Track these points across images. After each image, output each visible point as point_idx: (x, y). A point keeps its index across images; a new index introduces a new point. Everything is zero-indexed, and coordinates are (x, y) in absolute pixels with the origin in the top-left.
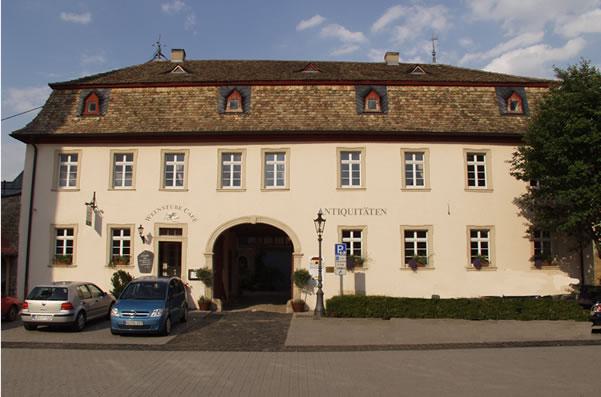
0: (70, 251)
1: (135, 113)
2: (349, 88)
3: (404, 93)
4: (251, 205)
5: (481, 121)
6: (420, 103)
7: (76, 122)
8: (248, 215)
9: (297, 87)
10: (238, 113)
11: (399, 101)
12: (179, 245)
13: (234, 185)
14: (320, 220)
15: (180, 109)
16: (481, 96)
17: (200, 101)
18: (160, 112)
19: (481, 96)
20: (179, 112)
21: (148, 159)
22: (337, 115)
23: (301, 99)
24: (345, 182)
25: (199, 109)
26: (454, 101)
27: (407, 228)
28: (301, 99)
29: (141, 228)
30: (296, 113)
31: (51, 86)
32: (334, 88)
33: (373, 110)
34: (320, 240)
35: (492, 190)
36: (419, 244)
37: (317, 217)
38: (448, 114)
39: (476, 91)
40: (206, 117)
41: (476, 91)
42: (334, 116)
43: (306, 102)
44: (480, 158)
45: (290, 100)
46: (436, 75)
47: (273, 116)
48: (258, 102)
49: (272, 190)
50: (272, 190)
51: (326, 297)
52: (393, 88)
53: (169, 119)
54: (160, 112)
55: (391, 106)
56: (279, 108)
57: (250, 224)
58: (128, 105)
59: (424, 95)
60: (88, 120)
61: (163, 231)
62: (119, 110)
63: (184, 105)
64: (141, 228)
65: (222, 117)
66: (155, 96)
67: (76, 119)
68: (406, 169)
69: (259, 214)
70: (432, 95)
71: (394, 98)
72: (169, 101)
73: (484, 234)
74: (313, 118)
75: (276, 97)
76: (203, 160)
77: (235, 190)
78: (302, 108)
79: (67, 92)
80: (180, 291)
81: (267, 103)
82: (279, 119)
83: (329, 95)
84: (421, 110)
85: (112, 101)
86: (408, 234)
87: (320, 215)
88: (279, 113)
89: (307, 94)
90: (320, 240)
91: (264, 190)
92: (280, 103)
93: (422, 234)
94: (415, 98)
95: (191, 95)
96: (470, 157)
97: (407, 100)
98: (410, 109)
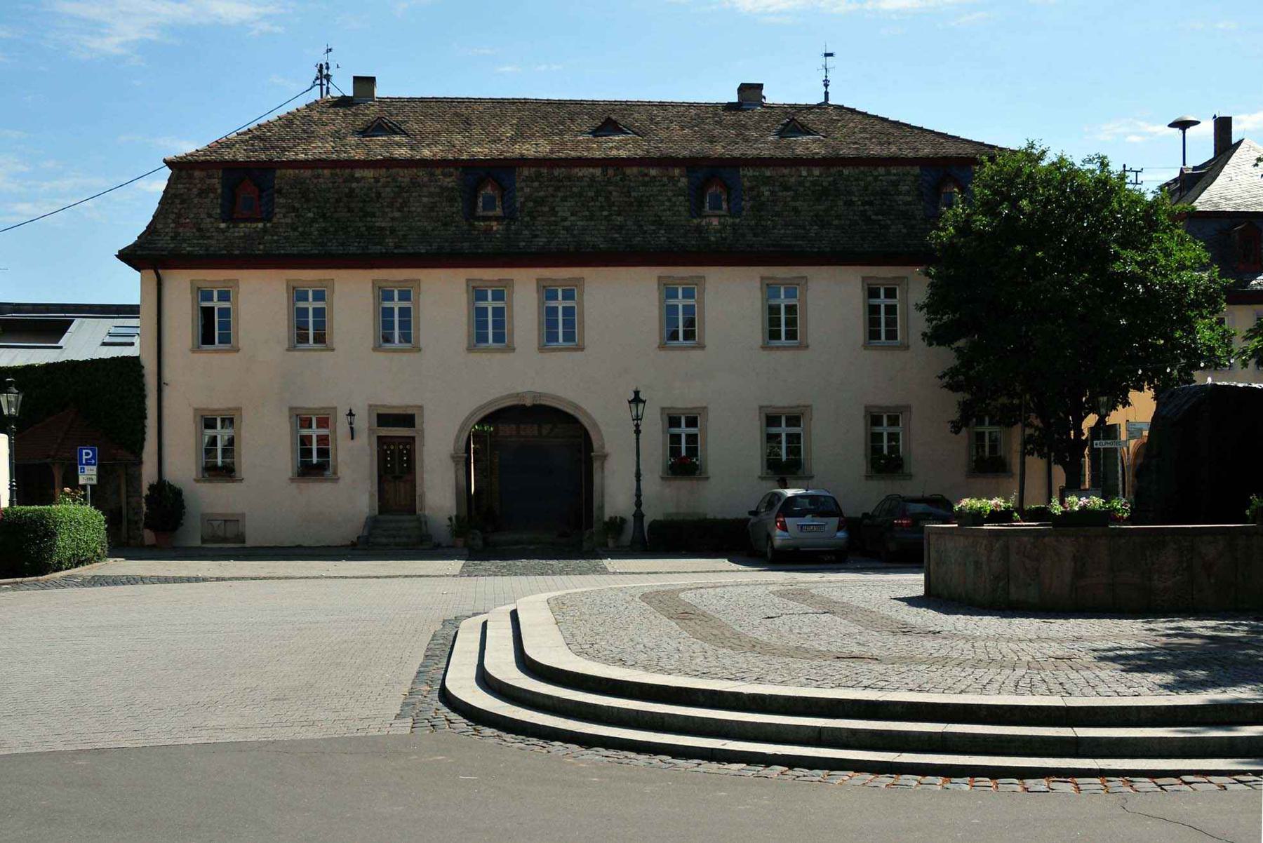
0: (323, 453)
1: (324, 216)
2: (677, 172)
3: (768, 181)
4: (527, 372)
5: (893, 229)
6: (794, 199)
7: (223, 231)
8: (520, 390)
9: (591, 170)
10: (497, 219)
11: (760, 195)
12: (413, 438)
13: (685, 338)
14: (637, 399)
15: (399, 210)
16: (895, 184)
17: (431, 195)
18: (366, 214)
19: (895, 184)
20: (397, 214)
21: (352, 295)
22: (659, 222)
23: (598, 194)
24: (303, 338)
25: (432, 209)
26: (850, 193)
27: (770, 411)
28: (598, 194)
29: (351, 414)
30: (591, 218)
31: (169, 163)
32: (653, 172)
33: (490, 214)
34: (638, 432)
35: (807, 347)
36: (688, 436)
37: (633, 396)
38: (838, 217)
39: (888, 173)
40: (445, 225)
41: (888, 173)
42: (653, 223)
43: (607, 199)
44: (890, 293)
45: (580, 195)
46: (416, 140)
47: (556, 223)
48: (528, 198)
49: (778, 348)
50: (778, 348)
51: (647, 520)
52: (751, 173)
53: (382, 229)
54: (366, 214)
55: (747, 204)
56: (563, 210)
57: (524, 406)
58: (308, 201)
59: (801, 184)
60: (243, 228)
61: (385, 419)
62: (294, 209)
63: (405, 203)
64: (351, 414)
65: (471, 225)
66: (354, 185)
67: (223, 225)
68: (668, 314)
69: (538, 387)
70: (814, 183)
71: (751, 189)
72: (379, 195)
73: (894, 421)
74: (621, 227)
75: (557, 189)
76: (442, 295)
77: (403, 351)
78: (602, 208)
79: (197, 173)
80: (779, 499)
81: (541, 202)
82: (566, 229)
83: (645, 184)
84: (795, 210)
85: (279, 191)
86: (772, 420)
87: (637, 393)
88: (565, 219)
89: (609, 182)
90: (638, 432)
91: (542, 349)
92: (564, 199)
93: (794, 420)
94: (786, 188)
95: (414, 183)
96: (479, 294)
97: (772, 192)
98: (777, 209)
